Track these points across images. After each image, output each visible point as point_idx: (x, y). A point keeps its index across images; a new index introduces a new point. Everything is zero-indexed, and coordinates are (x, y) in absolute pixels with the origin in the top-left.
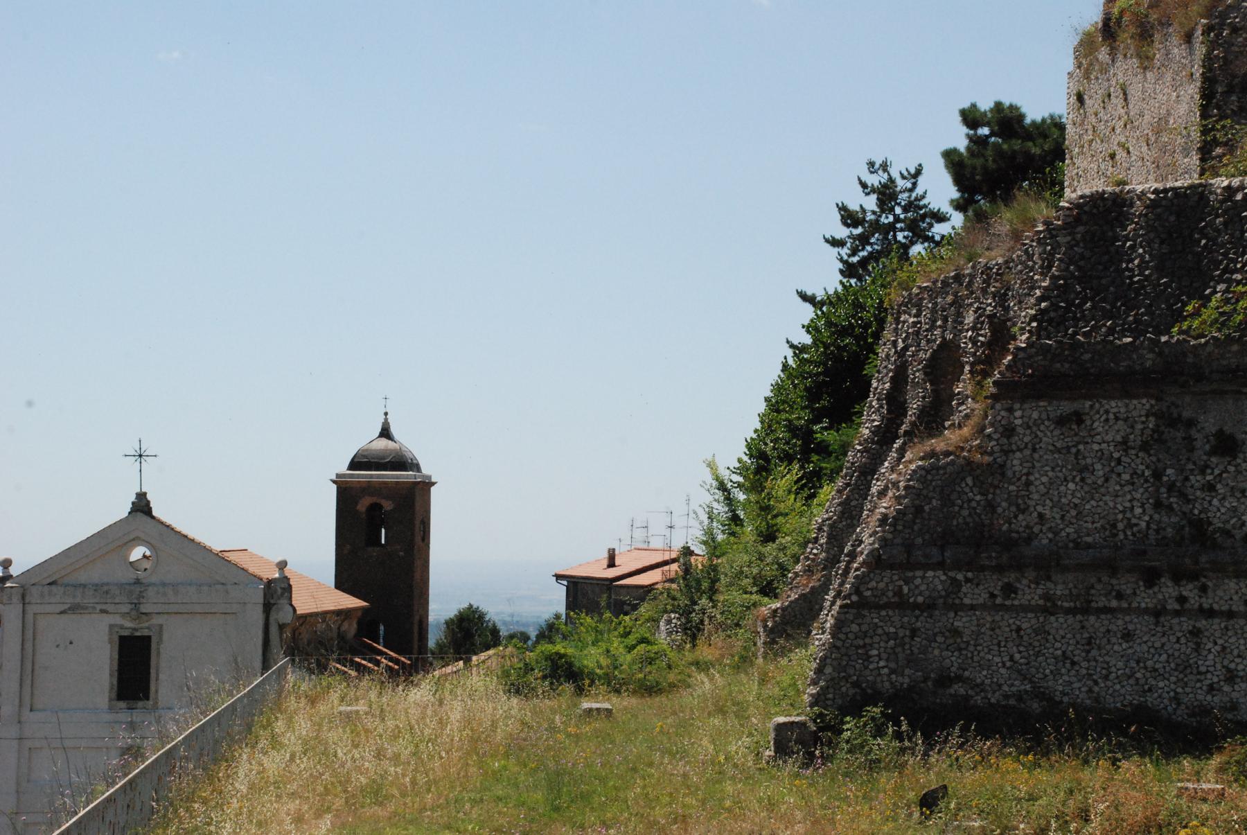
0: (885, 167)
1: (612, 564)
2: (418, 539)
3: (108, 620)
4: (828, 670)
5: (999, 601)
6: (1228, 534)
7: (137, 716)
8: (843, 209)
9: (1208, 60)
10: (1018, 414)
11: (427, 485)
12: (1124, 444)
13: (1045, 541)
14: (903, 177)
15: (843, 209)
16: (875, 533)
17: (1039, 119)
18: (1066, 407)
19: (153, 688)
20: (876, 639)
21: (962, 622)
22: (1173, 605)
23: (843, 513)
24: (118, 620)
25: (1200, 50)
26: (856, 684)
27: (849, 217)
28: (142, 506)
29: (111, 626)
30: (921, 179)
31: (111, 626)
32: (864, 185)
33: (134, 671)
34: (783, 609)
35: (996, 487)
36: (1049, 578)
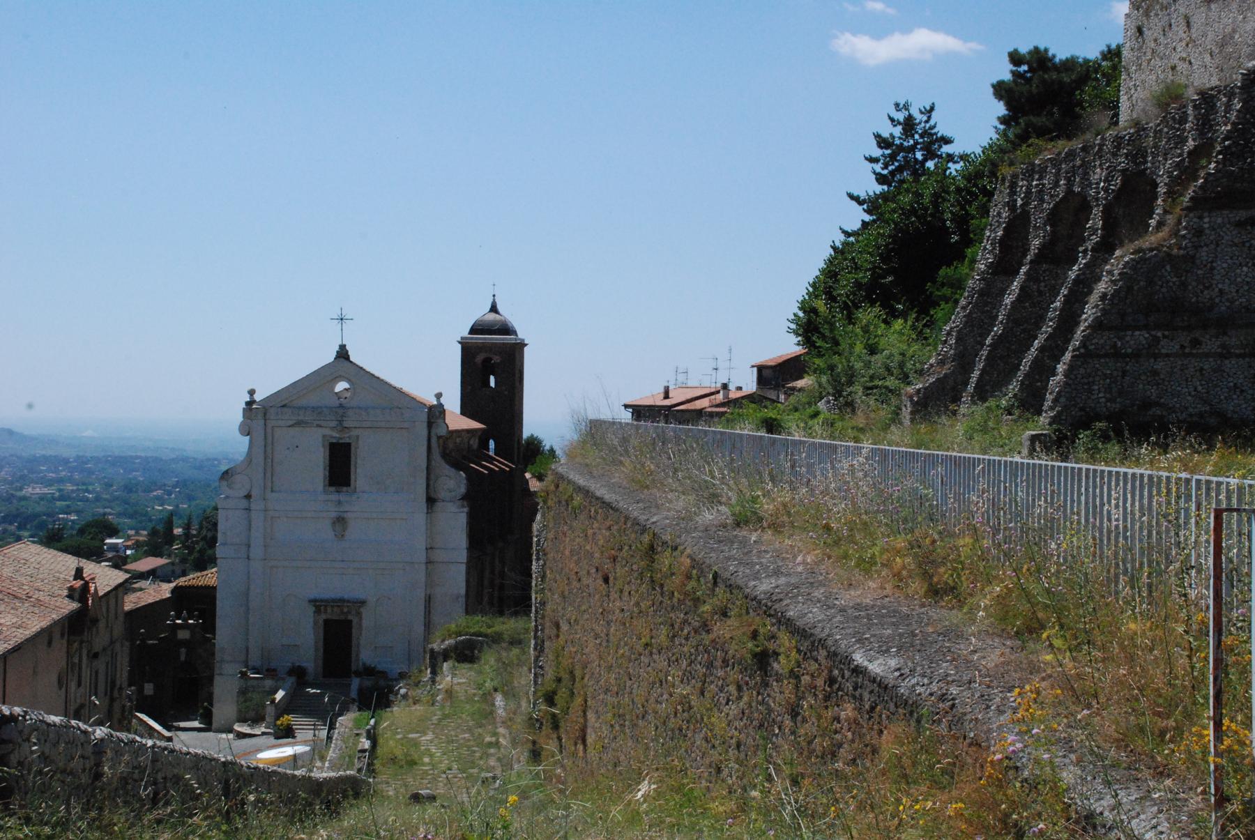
0: (906, 107)
1: (667, 396)
2: (517, 384)
3: (321, 431)
4: (1062, 400)
5: (1187, 350)
7: (342, 497)
8: (878, 136)
10: (1206, 220)
11: (522, 345)
13: (1223, 308)
14: (921, 112)
15: (878, 136)
16: (1097, 306)
17: (1064, 58)
19: (353, 477)
20: (1097, 378)
21: (1160, 365)
23: (966, 322)
24: (328, 432)
26: (1082, 409)
27: (882, 142)
28: (343, 354)
29: (324, 436)
30: (933, 114)
31: (324, 436)
32: (892, 120)
33: (340, 464)
34: (926, 389)
35: (1187, 272)
36: (1225, 334)
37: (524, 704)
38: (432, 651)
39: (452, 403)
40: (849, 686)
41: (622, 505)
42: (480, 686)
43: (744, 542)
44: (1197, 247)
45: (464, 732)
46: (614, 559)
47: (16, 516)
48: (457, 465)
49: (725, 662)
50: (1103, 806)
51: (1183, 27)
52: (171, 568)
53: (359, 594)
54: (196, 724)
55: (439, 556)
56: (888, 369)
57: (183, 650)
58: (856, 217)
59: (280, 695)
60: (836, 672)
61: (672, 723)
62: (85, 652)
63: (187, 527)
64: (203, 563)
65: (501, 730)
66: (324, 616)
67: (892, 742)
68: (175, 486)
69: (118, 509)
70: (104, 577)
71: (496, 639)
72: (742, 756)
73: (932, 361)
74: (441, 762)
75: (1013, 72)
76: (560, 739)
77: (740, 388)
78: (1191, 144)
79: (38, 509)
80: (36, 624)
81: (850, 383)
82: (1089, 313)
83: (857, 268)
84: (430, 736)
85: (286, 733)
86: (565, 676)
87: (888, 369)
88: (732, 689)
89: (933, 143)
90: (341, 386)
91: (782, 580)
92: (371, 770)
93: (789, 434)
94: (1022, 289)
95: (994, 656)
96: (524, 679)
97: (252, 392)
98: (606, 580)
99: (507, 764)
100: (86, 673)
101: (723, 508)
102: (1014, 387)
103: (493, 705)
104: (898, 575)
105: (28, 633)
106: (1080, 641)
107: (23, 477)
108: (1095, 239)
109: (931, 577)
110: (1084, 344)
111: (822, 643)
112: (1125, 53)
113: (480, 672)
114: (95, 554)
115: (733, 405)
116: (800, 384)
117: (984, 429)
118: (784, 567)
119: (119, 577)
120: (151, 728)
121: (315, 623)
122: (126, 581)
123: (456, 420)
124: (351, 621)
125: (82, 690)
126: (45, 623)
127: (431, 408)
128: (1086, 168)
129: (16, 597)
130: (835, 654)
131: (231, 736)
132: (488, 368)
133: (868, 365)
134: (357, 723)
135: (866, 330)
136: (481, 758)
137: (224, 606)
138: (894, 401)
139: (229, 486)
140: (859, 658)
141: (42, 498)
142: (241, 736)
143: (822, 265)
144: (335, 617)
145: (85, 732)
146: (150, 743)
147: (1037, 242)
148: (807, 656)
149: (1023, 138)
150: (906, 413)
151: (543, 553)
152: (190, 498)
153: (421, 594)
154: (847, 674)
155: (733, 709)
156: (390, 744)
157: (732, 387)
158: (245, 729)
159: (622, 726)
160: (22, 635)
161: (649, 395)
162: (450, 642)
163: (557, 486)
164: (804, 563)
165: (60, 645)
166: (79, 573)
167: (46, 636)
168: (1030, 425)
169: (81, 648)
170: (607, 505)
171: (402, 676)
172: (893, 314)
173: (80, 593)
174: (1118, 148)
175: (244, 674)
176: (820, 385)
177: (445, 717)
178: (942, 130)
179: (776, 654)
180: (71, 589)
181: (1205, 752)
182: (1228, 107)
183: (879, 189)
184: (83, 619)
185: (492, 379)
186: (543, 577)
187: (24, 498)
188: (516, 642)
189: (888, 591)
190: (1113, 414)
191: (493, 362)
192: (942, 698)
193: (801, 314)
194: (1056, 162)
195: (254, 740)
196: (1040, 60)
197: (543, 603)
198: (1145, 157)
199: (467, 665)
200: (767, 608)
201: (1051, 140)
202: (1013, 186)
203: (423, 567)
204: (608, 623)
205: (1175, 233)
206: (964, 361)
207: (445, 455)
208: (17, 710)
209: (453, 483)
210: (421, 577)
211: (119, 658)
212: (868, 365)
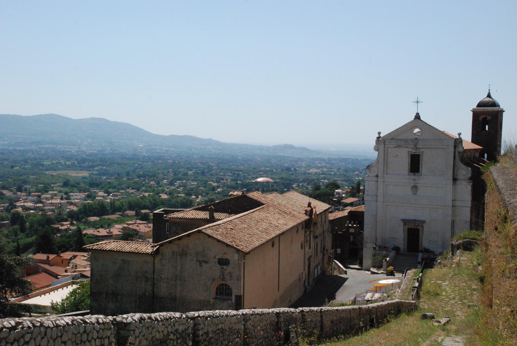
2: (499, 129)
7: (416, 177)
11: (502, 111)
24: (410, 150)
28: (418, 117)
31: (409, 152)
33: (415, 164)
38: (452, 245)
39: (467, 137)
45: (463, 282)
47: (306, 180)
48: (467, 164)
52: (359, 202)
54: (357, 267)
55: (458, 203)
62: (312, 236)
64: (362, 202)
66: (408, 227)
68: (363, 170)
69: (343, 179)
74: (450, 295)
79: (314, 177)
80: (291, 224)
84: (447, 283)
90: (416, 130)
97: (379, 133)
100: (312, 244)
105: (288, 227)
107: (309, 166)
120: (339, 267)
121: (404, 229)
124: (418, 230)
125: (310, 250)
126: (295, 224)
127: (456, 139)
129: (286, 213)
131: (369, 273)
132: (485, 122)
134: (415, 274)
136: (469, 295)
141: (316, 173)
142: (373, 273)
144: (412, 227)
153: (449, 219)
156: (428, 285)
158: (375, 270)
160: (285, 228)
162: (460, 241)
165: (302, 233)
166: (309, 205)
167: (296, 228)
169: (310, 235)
171: (441, 254)
173: (310, 213)
177: (455, 274)
180: (306, 211)
184: (310, 222)
185: (487, 126)
187: (309, 174)
195: (378, 275)
199: (468, 252)
203: (451, 208)
207: (463, 161)
209: (465, 172)
211: (326, 239)
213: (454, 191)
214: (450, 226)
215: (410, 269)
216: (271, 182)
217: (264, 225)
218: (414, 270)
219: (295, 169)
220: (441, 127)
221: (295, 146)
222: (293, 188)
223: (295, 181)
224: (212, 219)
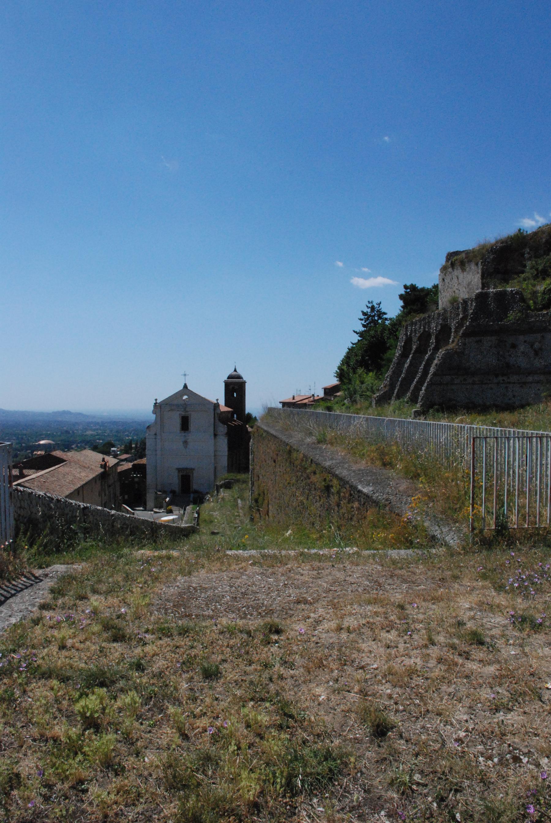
0: (372, 302)
1: (294, 399)
3: (179, 413)
6: (514, 365)
8: (363, 312)
9: (482, 269)
11: (245, 382)
12: (491, 347)
15: (363, 312)
18: (478, 338)
22: (502, 382)
25: (480, 267)
27: (364, 314)
28: (185, 386)
32: (367, 306)
37: (248, 503)
38: (217, 485)
39: (222, 402)
40: (357, 496)
41: (280, 436)
42: (233, 497)
43: (321, 449)
44: (464, 349)
46: (277, 455)
49: (315, 489)
50: (437, 533)
51: (456, 279)
53: (193, 467)
54: (141, 508)
56: (367, 389)
57: (136, 485)
58: (356, 338)
59: (168, 499)
60: (352, 492)
61: (298, 509)
63: (136, 444)
64: (142, 456)
65: (240, 511)
67: (371, 514)
70: (111, 461)
71: (238, 481)
72: (321, 519)
73: (382, 386)
75: (405, 292)
76: (260, 514)
77: (318, 396)
78: (461, 316)
80: (91, 476)
81: (355, 393)
82: (432, 370)
83: (356, 355)
85: (170, 512)
86: (262, 494)
87: (367, 389)
88: (318, 498)
89: (381, 314)
90: (185, 397)
91: (334, 461)
92: (198, 525)
93: (335, 411)
94: (411, 362)
95: (404, 485)
96: (248, 494)
97: (156, 400)
98: (275, 461)
99: (242, 522)
100: (107, 492)
101: (314, 437)
102: (409, 394)
103: (237, 503)
104: (372, 459)
106: (431, 480)
108: (433, 346)
109: (383, 459)
110: (430, 380)
111: (348, 482)
112: (440, 286)
113: (233, 492)
114: (108, 453)
115: (316, 402)
116: (338, 394)
117: (399, 409)
118: (333, 457)
119: (115, 461)
121: (178, 476)
122: (118, 462)
123: (223, 408)
126: (94, 476)
127: (215, 404)
128: (429, 322)
130: (352, 486)
131: (152, 512)
133: (361, 388)
134: (193, 509)
135: (360, 376)
137: (149, 470)
138: (370, 400)
139: (150, 431)
140: (360, 487)
141: (92, 435)
143: (345, 354)
145: (109, 512)
146: (128, 516)
147: (415, 347)
148: (342, 486)
149: (409, 313)
150: (374, 403)
151: (253, 452)
152: (137, 435)
154: (356, 492)
155: (318, 504)
156: (204, 515)
157: (315, 395)
158: (157, 510)
159: (281, 510)
161: (288, 398)
162: (222, 482)
163: (257, 430)
164: (341, 455)
165: (99, 482)
167: (94, 479)
168: (414, 407)
170: (275, 437)
171: (207, 493)
172: (370, 371)
173: (104, 466)
174: (439, 316)
175: (156, 493)
176: (345, 394)
177: (222, 507)
178: (383, 310)
179: (332, 486)
180: (101, 465)
181: (469, 515)
182: (471, 305)
183: (363, 329)
184: (105, 474)
185: (235, 394)
186: (253, 460)
188: (245, 482)
189: (369, 464)
190: (442, 403)
191: (235, 388)
192: (387, 500)
193: (338, 371)
194: (420, 321)
196: (413, 288)
197: (253, 469)
198: (447, 319)
199: (228, 490)
200: (329, 470)
201: (418, 314)
202: (407, 328)
204: (276, 476)
205: (458, 344)
206: (392, 386)
207: (220, 420)
208: (88, 505)
209: (223, 429)
210: (213, 461)
212: (361, 388)
213: (215, 445)
214: (213, 472)
215: (188, 505)
216: (53, 444)
217: (70, 478)
218: (191, 506)
219: (73, 432)
220: (203, 395)
221: (72, 411)
222: (72, 448)
223: (73, 442)
224: (22, 476)
